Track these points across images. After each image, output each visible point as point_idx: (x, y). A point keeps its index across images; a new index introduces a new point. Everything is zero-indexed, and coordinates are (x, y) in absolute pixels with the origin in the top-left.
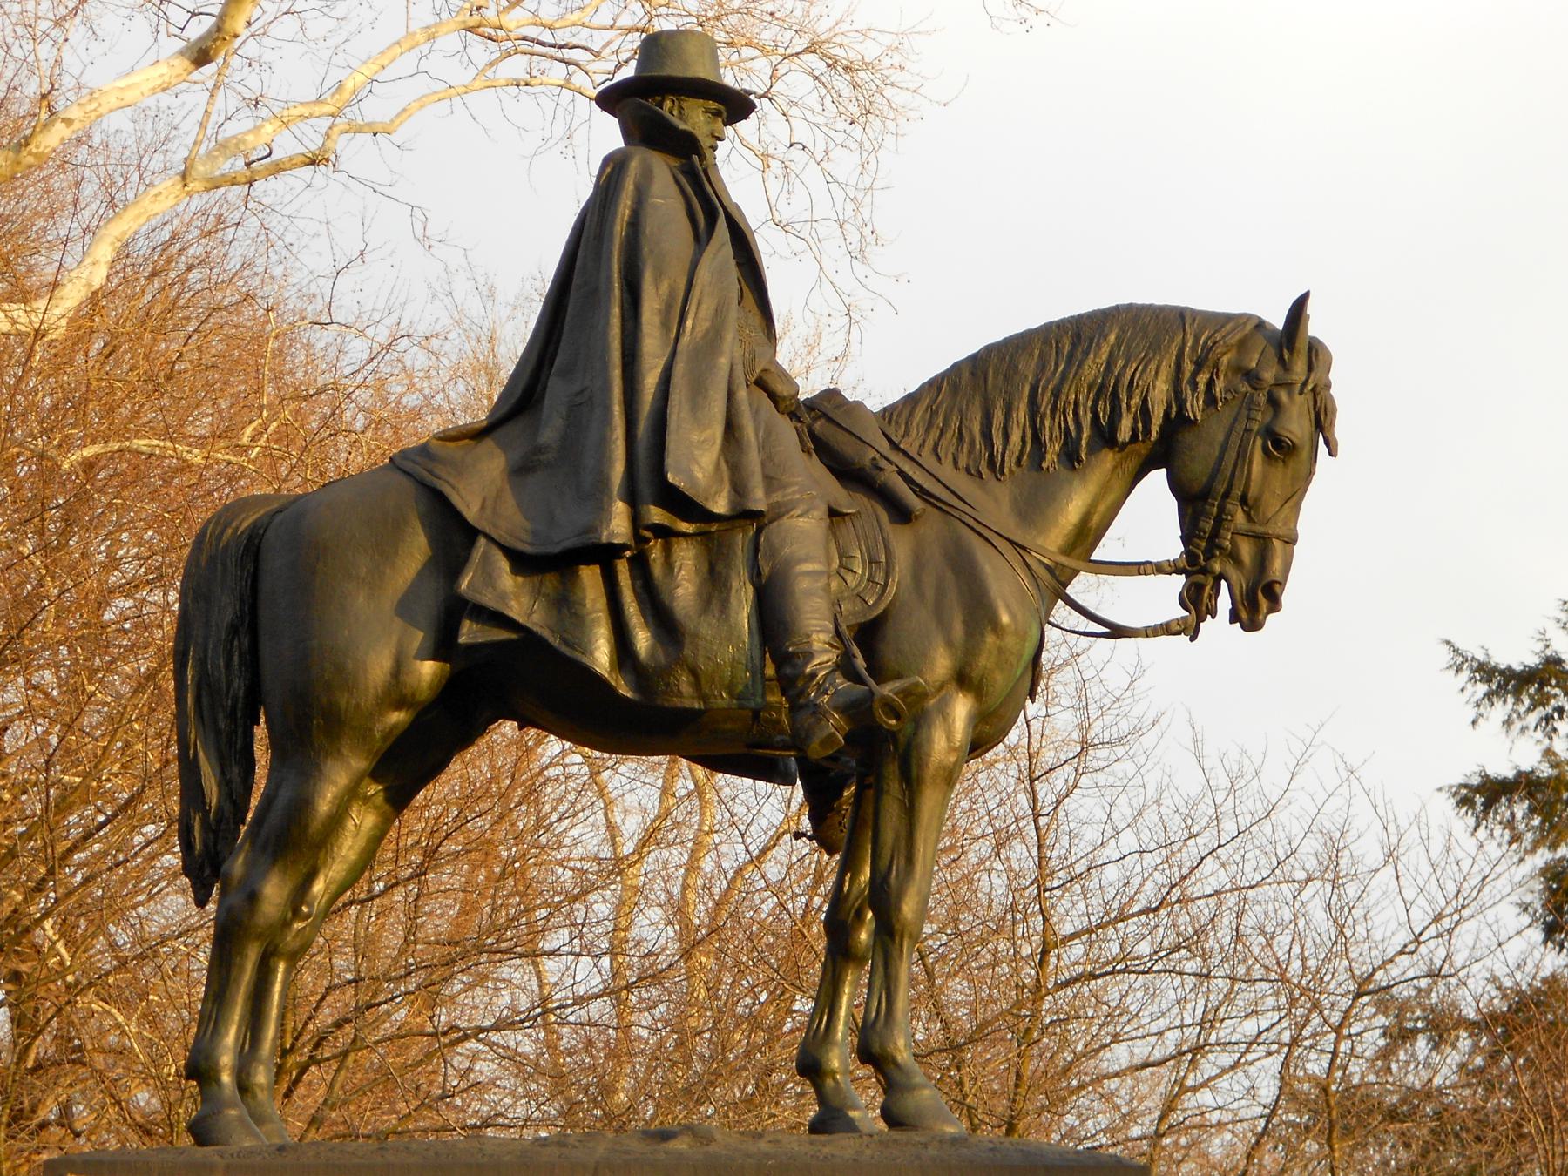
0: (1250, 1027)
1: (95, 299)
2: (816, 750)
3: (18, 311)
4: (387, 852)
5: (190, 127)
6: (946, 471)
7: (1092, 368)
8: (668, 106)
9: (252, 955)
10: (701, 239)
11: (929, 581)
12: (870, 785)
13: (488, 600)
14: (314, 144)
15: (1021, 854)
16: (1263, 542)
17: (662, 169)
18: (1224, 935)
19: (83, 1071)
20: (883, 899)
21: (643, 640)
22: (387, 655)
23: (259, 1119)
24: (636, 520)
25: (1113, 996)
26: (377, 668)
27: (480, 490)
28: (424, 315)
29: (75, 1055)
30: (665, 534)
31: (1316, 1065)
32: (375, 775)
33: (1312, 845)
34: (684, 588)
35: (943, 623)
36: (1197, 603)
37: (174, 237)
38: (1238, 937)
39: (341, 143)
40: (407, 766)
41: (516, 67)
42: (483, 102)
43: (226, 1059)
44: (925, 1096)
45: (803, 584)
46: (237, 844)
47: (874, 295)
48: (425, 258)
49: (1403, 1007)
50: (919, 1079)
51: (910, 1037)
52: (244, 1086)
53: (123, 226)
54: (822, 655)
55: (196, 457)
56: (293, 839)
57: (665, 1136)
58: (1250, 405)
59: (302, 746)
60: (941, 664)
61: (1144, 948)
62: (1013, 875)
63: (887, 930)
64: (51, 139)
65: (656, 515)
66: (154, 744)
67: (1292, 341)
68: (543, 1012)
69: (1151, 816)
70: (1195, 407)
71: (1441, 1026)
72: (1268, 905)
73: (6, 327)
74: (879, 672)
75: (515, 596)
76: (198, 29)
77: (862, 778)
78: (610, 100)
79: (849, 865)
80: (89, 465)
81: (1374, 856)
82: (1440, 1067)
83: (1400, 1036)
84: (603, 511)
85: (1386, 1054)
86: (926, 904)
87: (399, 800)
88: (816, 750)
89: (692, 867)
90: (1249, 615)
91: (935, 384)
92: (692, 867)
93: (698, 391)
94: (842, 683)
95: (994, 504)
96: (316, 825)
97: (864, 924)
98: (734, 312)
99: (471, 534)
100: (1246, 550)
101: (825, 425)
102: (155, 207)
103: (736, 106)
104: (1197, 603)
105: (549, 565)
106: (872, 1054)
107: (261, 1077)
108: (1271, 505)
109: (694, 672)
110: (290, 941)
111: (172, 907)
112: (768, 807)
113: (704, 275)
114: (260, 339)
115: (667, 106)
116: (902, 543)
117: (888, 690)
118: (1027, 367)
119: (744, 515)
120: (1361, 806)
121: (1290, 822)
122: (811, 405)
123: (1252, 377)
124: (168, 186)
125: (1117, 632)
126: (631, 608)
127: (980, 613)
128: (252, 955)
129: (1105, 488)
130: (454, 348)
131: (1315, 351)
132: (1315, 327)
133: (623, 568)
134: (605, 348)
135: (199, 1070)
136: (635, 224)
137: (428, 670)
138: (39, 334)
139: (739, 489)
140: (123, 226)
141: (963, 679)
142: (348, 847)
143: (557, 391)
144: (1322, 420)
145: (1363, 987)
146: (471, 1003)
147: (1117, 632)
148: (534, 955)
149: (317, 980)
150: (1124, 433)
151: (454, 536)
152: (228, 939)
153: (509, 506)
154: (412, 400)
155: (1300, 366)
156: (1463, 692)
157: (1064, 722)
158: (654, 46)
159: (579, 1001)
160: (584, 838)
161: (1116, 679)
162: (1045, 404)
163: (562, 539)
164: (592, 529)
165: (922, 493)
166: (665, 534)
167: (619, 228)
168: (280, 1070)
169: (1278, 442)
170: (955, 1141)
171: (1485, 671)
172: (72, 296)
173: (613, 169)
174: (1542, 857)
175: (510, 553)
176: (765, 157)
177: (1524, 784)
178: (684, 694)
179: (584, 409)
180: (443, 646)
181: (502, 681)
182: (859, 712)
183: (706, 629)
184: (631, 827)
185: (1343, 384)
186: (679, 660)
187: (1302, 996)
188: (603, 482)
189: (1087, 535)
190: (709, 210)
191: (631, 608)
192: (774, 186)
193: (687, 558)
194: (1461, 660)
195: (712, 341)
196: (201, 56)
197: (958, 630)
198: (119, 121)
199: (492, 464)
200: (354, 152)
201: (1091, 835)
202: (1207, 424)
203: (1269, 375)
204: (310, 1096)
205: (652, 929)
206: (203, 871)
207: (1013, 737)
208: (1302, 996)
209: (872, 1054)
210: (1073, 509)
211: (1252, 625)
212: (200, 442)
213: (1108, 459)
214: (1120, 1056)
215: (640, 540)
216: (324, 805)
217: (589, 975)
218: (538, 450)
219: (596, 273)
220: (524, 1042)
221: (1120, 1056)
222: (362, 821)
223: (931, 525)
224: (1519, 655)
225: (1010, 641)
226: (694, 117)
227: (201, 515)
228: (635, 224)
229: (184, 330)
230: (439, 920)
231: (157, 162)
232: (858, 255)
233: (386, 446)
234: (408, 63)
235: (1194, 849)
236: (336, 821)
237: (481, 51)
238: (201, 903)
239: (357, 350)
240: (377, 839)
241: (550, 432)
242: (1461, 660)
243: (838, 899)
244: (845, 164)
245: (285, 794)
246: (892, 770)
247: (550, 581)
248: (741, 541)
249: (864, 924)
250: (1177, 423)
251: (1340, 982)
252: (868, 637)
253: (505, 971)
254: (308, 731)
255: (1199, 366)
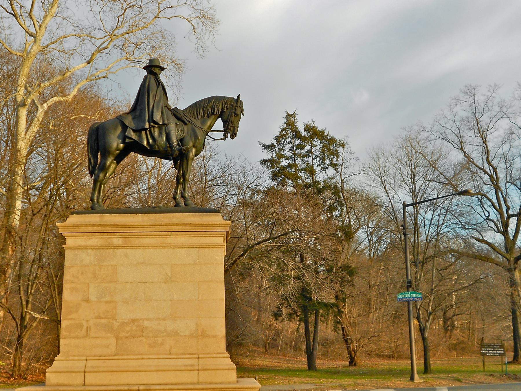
0: (233, 193)
1: (75, 96)
2: (174, 156)
3: (64, 98)
4: (117, 170)
5: (88, 72)
6: (191, 118)
7: (211, 104)
8: (153, 69)
9: (99, 184)
10: (158, 87)
11: (189, 133)
12: (182, 161)
13: (130, 136)
14: (105, 75)
15: (202, 170)
16: (234, 127)
17: (152, 77)
18: (229, 180)
19: (76, 201)
20: (184, 176)
21: (151, 141)
22: (116, 143)
23: (100, 206)
24: (150, 125)
25: (215, 189)
26: (115, 145)
27: (128, 121)
28: (120, 98)
29: (74, 199)
30: (153, 127)
31: (242, 197)
32: (115, 160)
33: (241, 168)
34: (156, 134)
35: (191, 138)
36: (225, 136)
37: (86, 88)
38: (231, 180)
39: (108, 75)
40: (119, 159)
41: (132, 64)
42: (128, 69)
43: (95, 198)
44: (190, 202)
45: (172, 133)
46: (96, 169)
47: (181, 96)
48: (121, 91)
49: (253, 190)
50: (189, 199)
51: (188, 194)
52: (98, 202)
53: (79, 86)
54: (175, 143)
55: (89, 117)
56: (104, 168)
57: (155, 207)
58: (232, 109)
59: (105, 156)
60: (191, 144)
61: (219, 182)
62: (201, 173)
63: (184, 180)
64: (68, 74)
65: (152, 124)
66: (85, 156)
67: (238, 101)
68: (139, 191)
69: (220, 165)
70: (225, 109)
71: (258, 192)
72: (235, 176)
73: (79, 1)
74: (183, 145)
75: (134, 136)
76: (88, 59)
77: (181, 159)
78: (145, 68)
79: (179, 171)
80: (75, 119)
81: (249, 170)
82: (259, 198)
83: (253, 194)
84: (145, 124)
85: (251, 196)
86: (190, 177)
87: (118, 163)
88: (174, 156)
89: (158, 173)
90: (232, 137)
91: (190, 106)
92: (158, 173)
93: (158, 108)
94: (178, 147)
95: (198, 123)
96: (107, 166)
97: (181, 179)
98: (162, 97)
99: (127, 127)
100: (232, 129)
101: (175, 113)
102: (83, 83)
103: (162, 69)
104: (225, 136)
105: (138, 131)
106: (183, 196)
107: (100, 201)
108: (235, 123)
109: (158, 146)
110: (104, 182)
111: (88, 179)
112: (168, 164)
113: (158, 92)
114: (97, 101)
115: (153, 69)
116: (186, 128)
117: (184, 148)
118: (202, 104)
119: (164, 124)
120: (248, 164)
121: (238, 165)
122: (173, 109)
123: (232, 105)
124: (85, 80)
125: (215, 140)
126: (149, 137)
127: (196, 137)
128: (99, 184)
129: (213, 120)
130: (125, 102)
131: (241, 101)
132: (241, 99)
133: (148, 131)
134: (145, 102)
135: (92, 200)
136: (149, 85)
137: (122, 145)
138: (67, 101)
139: (163, 121)
140: (79, 86)
141: (194, 146)
142: (111, 170)
143: (138, 108)
144: (242, 111)
145: (248, 187)
146: (128, 191)
147: (215, 140)
148: (137, 184)
149: (107, 188)
150: (215, 113)
151: (125, 127)
152: (95, 182)
153: (132, 123)
154: (119, 110)
155: (239, 104)
156: (261, 148)
157: (208, 152)
158: (151, 60)
159: (144, 190)
160: (144, 169)
161: (215, 147)
162: (205, 109)
163: (140, 128)
164: (144, 126)
165: (188, 121)
166: (153, 127)
167: (147, 86)
168: (103, 200)
169: (236, 114)
170: (194, 207)
171: (264, 145)
172: (72, 96)
173: (146, 77)
174: (272, 170)
175: (132, 129)
176: (166, 77)
177: (269, 160)
178: (156, 148)
179: (142, 110)
180: (124, 142)
181: (132, 147)
182: (180, 151)
183: (159, 139)
184: (150, 167)
185: (244, 106)
186: (156, 144)
187: (240, 188)
188: (145, 120)
189: (211, 127)
190: (159, 83)
191: (149, 137)
192: (167, 80)
193: (156, 130)
194: (261, 144)
195: (159, 101)
196: (89, 63)
197: (193, 139)
198: (78, 72)
199: (130, 117)
200: (110, 76)
201: (212, 167)
202: (227, 112)
203: (235, 105)
204: (107, 204)
205: (153, 181)
206: (92, 173)
207: (201, 154)
208: (240, 188)
209: (183, 196)
210: (209, 123)
211: (233, 139)
212: (90, 116)
213: (213, 116)
214: (216, 196)
215: (150, 128)
216: (108, 164)
217: (144, 187)
218: (136, 116)
219: (143, 92)
220: (136, 196)
221: (216, 196)
222: (113, 166)
223: (189, 126)
224: (268, 143)
225: (200, 141)
226: (157, 70)
227: (90, 124)
228: (149, 85)
229: (87, 100)
230: (124, 180)
231: (83, 77)
232: (179, 91)
233: (115, 116)
234: (117, 64)
235: (225, 169)
236: (110, 166)
237: (127, 62)
238: (91, 177)
239: (111, 103)
240: (115, 168)
241: (137, 113)
242: (261, 144)
243: (178, 176)
244: (177, 78)
245: (103, 162)
246: (185, 158)
247: (138, 133)
248: (164, 128)
249: (181, 179)
250: (222, 112)
251: (244, 187)
252: (181, 140)
253: (133, 186)
254: (106, 153)
255: (225, 104)
